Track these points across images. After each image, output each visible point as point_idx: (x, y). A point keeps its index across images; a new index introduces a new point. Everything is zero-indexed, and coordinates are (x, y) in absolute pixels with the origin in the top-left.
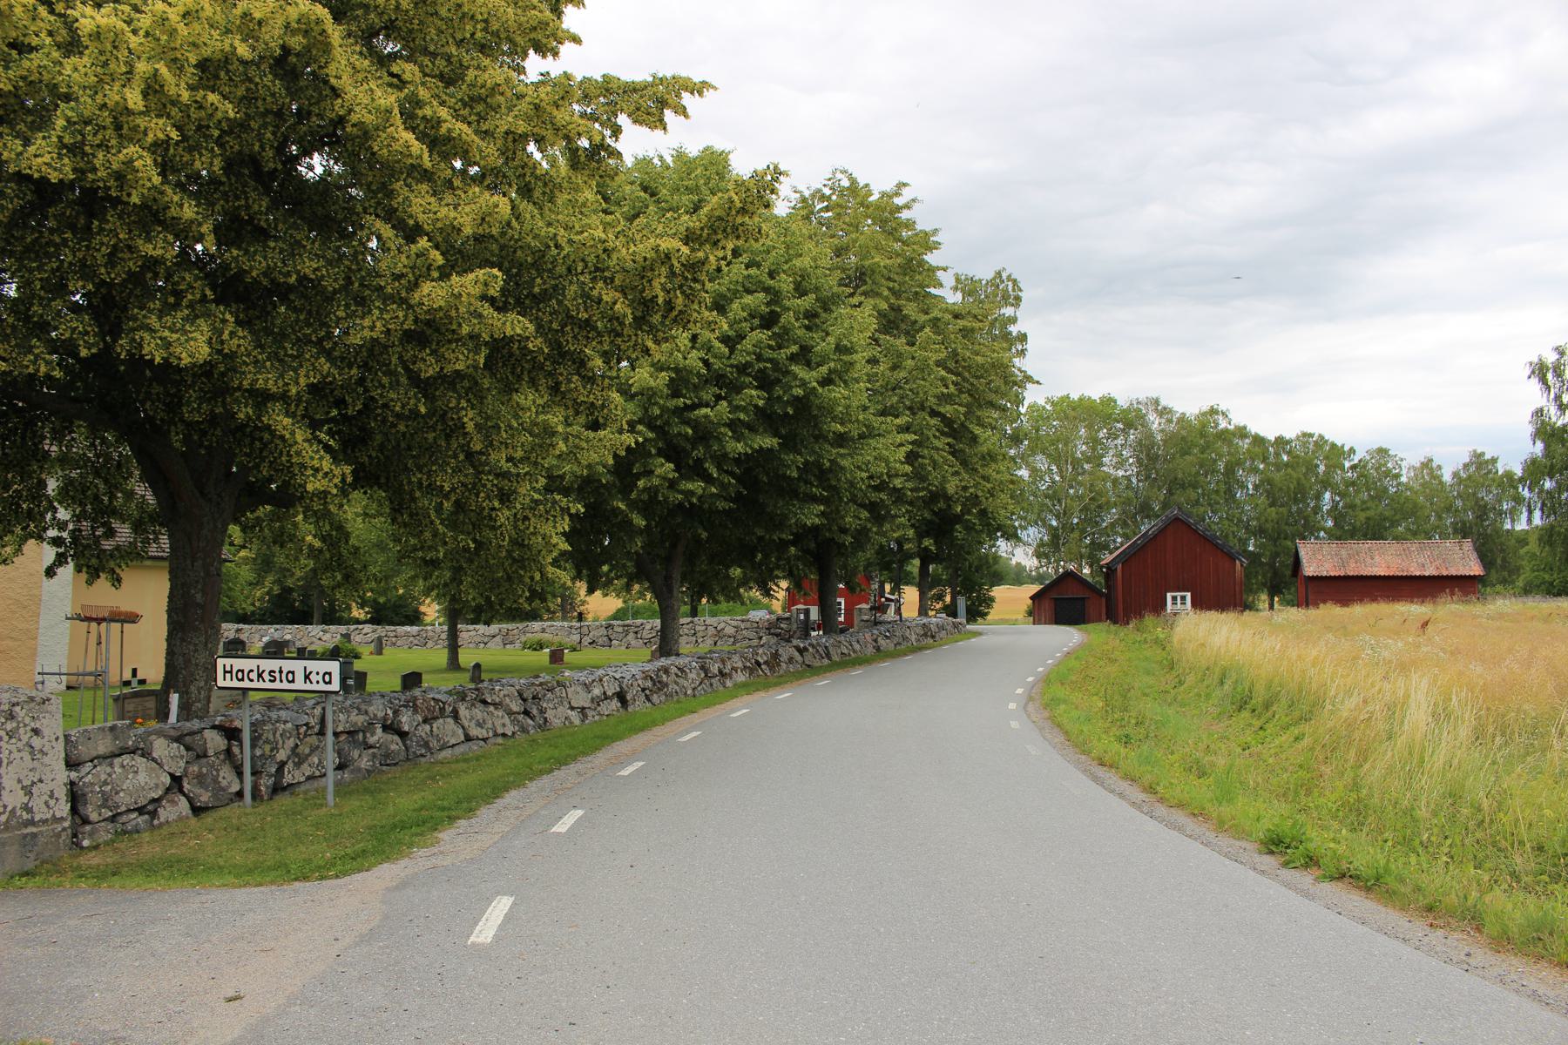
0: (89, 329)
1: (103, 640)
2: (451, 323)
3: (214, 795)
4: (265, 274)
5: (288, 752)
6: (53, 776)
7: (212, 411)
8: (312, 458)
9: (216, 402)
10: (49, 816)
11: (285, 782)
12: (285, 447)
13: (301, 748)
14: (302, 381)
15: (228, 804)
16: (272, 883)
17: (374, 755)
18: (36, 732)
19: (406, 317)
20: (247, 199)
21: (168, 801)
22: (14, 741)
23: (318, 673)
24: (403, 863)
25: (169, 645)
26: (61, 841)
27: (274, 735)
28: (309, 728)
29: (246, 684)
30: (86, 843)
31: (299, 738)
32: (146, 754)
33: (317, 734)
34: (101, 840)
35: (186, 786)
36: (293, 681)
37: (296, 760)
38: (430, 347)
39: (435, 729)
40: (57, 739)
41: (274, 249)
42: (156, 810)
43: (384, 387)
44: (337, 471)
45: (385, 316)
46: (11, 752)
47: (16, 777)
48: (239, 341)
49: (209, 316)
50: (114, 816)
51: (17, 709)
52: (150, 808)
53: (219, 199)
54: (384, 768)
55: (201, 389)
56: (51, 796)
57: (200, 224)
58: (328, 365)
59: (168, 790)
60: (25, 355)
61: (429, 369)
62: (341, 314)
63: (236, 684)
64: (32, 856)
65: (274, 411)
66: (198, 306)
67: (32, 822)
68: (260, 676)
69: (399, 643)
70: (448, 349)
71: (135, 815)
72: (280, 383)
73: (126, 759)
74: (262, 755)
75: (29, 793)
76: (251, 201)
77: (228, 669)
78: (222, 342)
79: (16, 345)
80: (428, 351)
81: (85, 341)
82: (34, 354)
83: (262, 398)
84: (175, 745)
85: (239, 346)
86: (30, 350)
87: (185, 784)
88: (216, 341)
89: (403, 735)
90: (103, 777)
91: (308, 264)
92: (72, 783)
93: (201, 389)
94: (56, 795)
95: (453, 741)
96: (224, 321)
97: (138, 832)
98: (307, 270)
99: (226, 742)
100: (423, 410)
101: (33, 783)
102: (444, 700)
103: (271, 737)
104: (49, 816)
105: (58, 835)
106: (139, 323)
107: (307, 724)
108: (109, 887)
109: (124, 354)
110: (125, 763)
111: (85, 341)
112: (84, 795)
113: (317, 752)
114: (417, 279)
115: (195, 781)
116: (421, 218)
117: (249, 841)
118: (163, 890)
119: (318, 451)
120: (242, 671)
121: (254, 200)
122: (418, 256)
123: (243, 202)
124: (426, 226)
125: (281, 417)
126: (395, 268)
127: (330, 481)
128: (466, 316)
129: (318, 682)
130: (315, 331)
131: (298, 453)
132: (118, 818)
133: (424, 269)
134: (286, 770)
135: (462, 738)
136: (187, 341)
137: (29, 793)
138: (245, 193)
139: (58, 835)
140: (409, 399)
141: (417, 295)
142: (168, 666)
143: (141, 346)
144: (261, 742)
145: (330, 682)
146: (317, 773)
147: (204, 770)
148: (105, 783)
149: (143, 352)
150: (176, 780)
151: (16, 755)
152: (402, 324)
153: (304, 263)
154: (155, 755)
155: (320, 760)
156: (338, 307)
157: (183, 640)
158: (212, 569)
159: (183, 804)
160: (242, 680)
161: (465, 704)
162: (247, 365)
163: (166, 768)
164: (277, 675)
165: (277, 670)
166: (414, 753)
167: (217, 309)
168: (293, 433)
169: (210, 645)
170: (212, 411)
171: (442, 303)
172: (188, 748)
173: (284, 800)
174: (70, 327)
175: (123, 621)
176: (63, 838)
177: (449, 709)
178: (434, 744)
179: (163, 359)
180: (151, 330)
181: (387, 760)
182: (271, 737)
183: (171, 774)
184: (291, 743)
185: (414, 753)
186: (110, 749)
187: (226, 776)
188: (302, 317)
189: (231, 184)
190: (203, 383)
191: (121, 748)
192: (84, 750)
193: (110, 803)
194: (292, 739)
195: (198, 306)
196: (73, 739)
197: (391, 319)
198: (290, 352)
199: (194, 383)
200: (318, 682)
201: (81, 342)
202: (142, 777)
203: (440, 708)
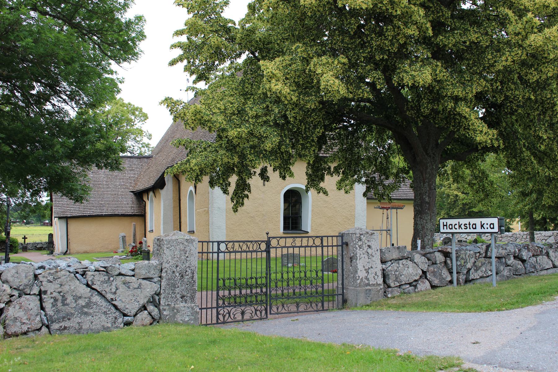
0: (381, 77)
1: (389, 217)
2: (544, 54)
3: (440, 281)
4: (454, 45)
5: (472, 264)
6: (376, 266)
7: (433, 108)
8: (479, 126)
9: (435, 104)
10: (375, 283)
11: (471, 278)
12: (467, 122)
13: (477, 264)
14: (474, 91)
15: (446, 286)
16: (475, 312)
17: (510, 270)
18: (369, 246)
19: (522, 52)
20: (442, 12)
21: (421, 282)
22: (361, 250)
23: (487, 224)
24: (539, 307)
25: (415, 220)
26: (380, 293)
27: (465, 255)
28: (480, 254)
29: (453, 230)
30: (389, 296)
31: (476, 258)
32: (412, 260)
33: (484, 257)
34: (395, 295)
35: (428, 276)
36: (475, 228)
37: (475, 268)
38: (534, 67)
39: (538, 260)
40: (377, 250)
41: (457, 33)
42: (416, 285)
43: (512, 90)
44: (490, 132)
45: (512, 54)
46: (360, 254)
47: (362, 265)
48: (443, 74)
49: (430, 64)
50: (400, 286)
51: (362, 236)
52: (414, 283)
53: (431, 15)
54: (515, 276)
55: (428, 99)
56: (376, 274)
57: (426, 24)
58: (485, 82)
59: (421, 277)
60: (359, 90)
61: (534, 77)
62: (490, 57)
63: (449, 231)
64: (369, 299)
65: (461, 105)
66: (425, 61)
67: (368, 285)
68: (460, 226)
69: (503, 240)
70: (543, 67)
71: (408, 286)
72: (464, 92)
73: (404, 261)
74: (460, 265)
75: (368, 272)
76: (444, 13)
77: (445, 224)
78: (436, 75)
79: (355, 86)
80: (533, 69)
81: (379, 82)
82: (362, 89)
83: (456, 99)
84: (423, 257)
85: (444, 76)
86: (360, 87)
87: (428, 275)
88: (434, 73)
89: (523, 261)
90: (395, 268)
91: (473, 36)
92: (383, 270)
93: (428, 99)
94: (377, 274)
95: (547, 267)
96: (437, 66)
97: (409, 293)
98: (473, 38)
99: (444, 258)
100: (533, 97)
101: (369, 268)
102: (542, 247)
103: (464, 257)
104: (375, 283)
105: (379, 291)
106: (401, 70)
107: (479, 252)
108: (402, 311)
109: (396, 84)
110: (404, 263)
111: (379, 82)
112: (388, 275)
113: (484, 266)
114: (527, 34)
115: (432, 274)
116: (527, 4)
117: (460, 297)
118: (426, 312)
119: (482, 123)
120: (452, 225)
121: (446, 12)
122: (527, 22)
123: (441, 14)
124: (530, 8)
125: (465, 108)
126: (516, 30)
127: (488, 136)
128: (552, 49)
129: (487, 228)
130: (478, 68)
131: (473, 124)
132: (402, 286)
133: (530, 28)
134: (471, 272)
135: (552, 266)
136: (422, 74)
137: (368, 272)
138: (441, 9)
139: (379, 291)
140: (525, 93)
141: (528, 42)
142: (414, 229)
143: (403, 79)
144: (460, 258)
145: (493, 228)
146: (485, 275)
147: (436, 270)
148: (396, 271)
149: (404, 82)
150: (424, 273)
151: (362, 256)
152: (521, 57)
153: (472, 36)
154: (415, 261)
155: (486, 269)
156: (488, 54)
157: (421, 218)
158: (432, 186)
159: (427, 284)
160: (452, 229)
161: (552, 250)
162: (449, 86)
163: (420, 267)
164: (468, 226)
165: (468, 223)
166: (529, 270)
167: (434, 62)
168: (470, 115)
169: (432, 221)
170: (433, 108)
171: (541, 43)
172: (429, 260)
173: (469, 286)
174: (373, 77)
175: (397, 208)
176: (381, 293)
177: (544, 252)
178: (538, 267)
179: (412, 84)
180: (406, 72)
181: (517, 273)
182: (464, 257)
183: (422, 270)
184: (473, 260)
185: (529, 270)
186: (398, 256)
187: (445, 273)
188: (471, 62)
189: (435, 7)
190: (428, 96)
191: (402, 257)
192: (388, 256)
193: (398, 280)
194: (473, 259)
195: (425, 61)
196: (383, 251)
197: (515, 55)
198: (467, 79)
199: (425, 97)
200: (487, 228)
201: (377, 83)
202: (411, 270)
203: (540, 251)
